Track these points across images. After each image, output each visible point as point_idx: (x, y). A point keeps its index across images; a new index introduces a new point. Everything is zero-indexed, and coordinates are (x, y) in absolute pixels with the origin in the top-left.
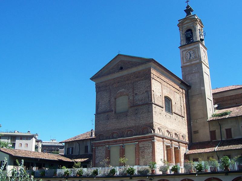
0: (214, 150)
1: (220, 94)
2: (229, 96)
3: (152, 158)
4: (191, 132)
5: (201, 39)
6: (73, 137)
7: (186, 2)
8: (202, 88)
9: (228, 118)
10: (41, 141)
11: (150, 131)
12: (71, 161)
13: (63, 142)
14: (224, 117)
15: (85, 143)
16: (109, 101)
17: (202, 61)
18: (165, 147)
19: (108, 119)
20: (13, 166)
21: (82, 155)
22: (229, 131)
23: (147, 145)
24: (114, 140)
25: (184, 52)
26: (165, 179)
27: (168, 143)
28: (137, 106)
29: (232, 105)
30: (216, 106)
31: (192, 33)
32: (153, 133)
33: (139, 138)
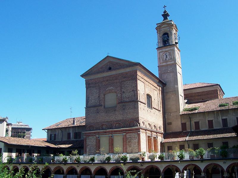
0: (186, 140)
1: (190, 90)
2: (197, 93)
3: (138, 147)
4: (166, 124)
5: (176, 42)
6: (54, 123)
7: (164, 7)
8: (176, 86)
9: (197, 113)
10: (11, 124)
11: (136, 124)
12: (56, 147)
13: (45, 129)
14: (194, 112)
15: (67, 130)
16: (99, 96)
17: (177, 62)
18: (147, 137)
19: (98, 112)
20: (7, 153)
21: (65, 141)
22: (197, 124)
23: (134, 136)
24: (103, 131)
25: (160, 53)
26: (153, 165)
27: (149, 134)
28: (125, 102)
29: (199, 100)
30: (186, 101)
31: (168, 37)
32: (139, 126)
33: (126, 130)
